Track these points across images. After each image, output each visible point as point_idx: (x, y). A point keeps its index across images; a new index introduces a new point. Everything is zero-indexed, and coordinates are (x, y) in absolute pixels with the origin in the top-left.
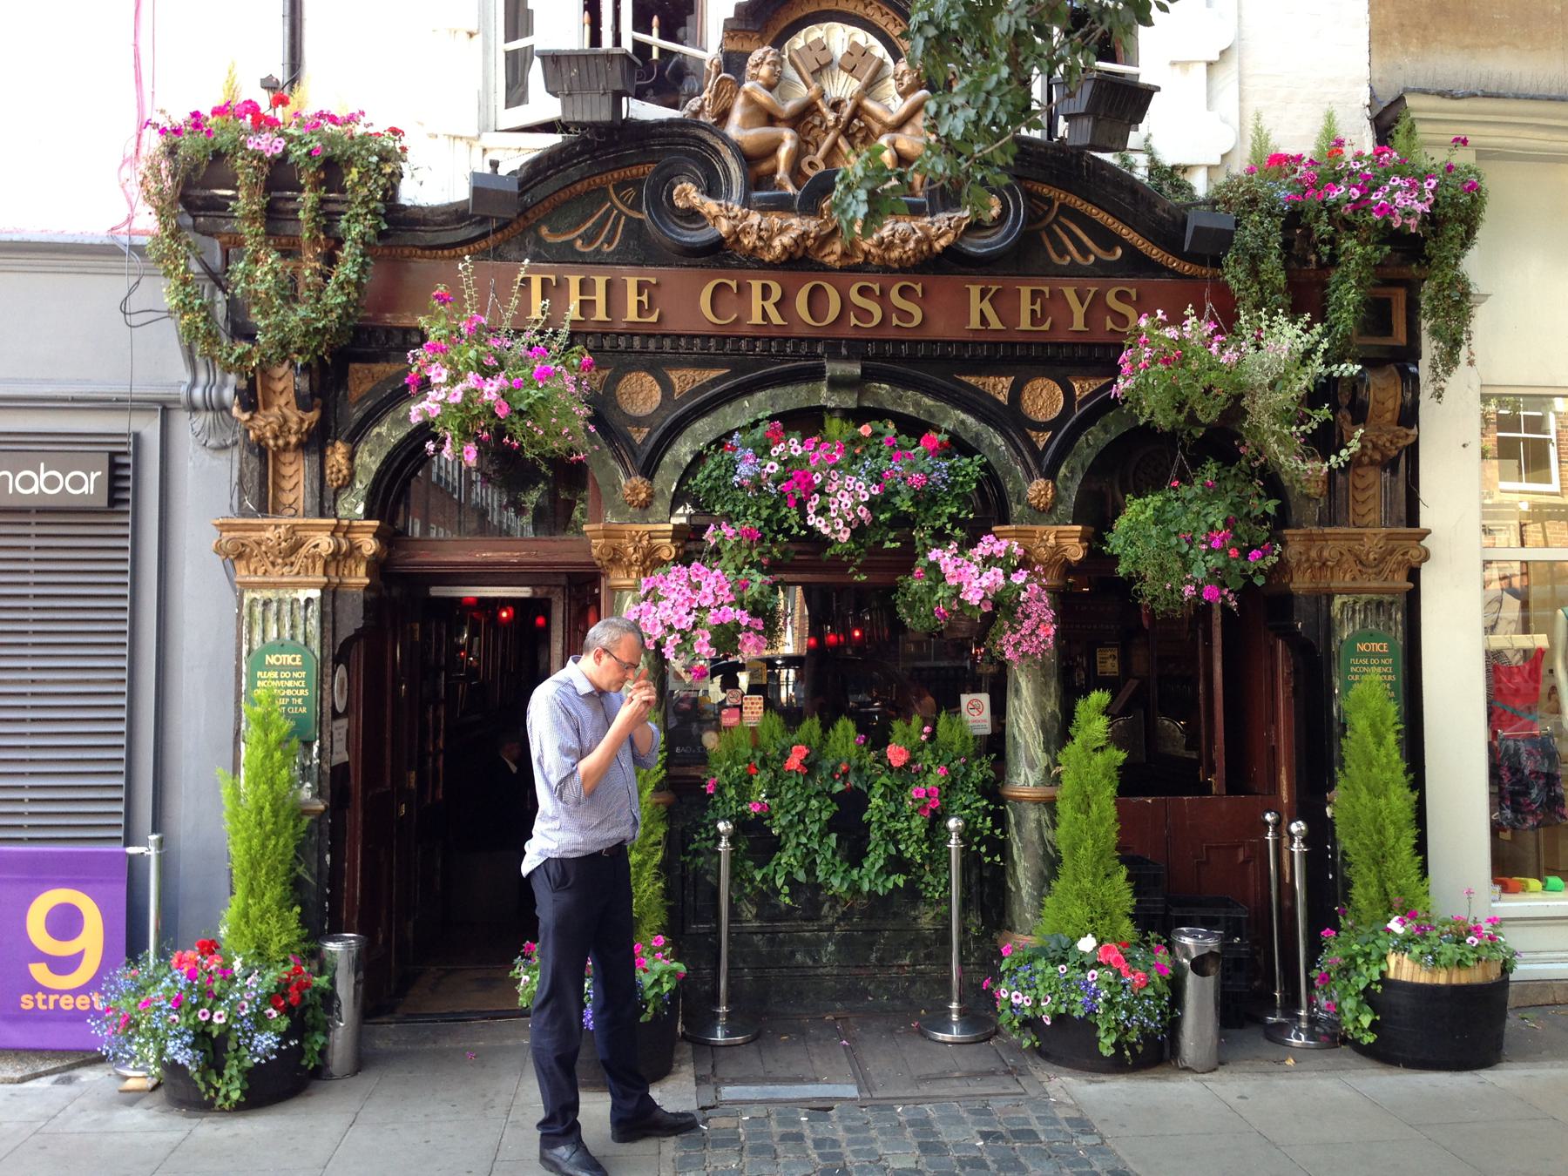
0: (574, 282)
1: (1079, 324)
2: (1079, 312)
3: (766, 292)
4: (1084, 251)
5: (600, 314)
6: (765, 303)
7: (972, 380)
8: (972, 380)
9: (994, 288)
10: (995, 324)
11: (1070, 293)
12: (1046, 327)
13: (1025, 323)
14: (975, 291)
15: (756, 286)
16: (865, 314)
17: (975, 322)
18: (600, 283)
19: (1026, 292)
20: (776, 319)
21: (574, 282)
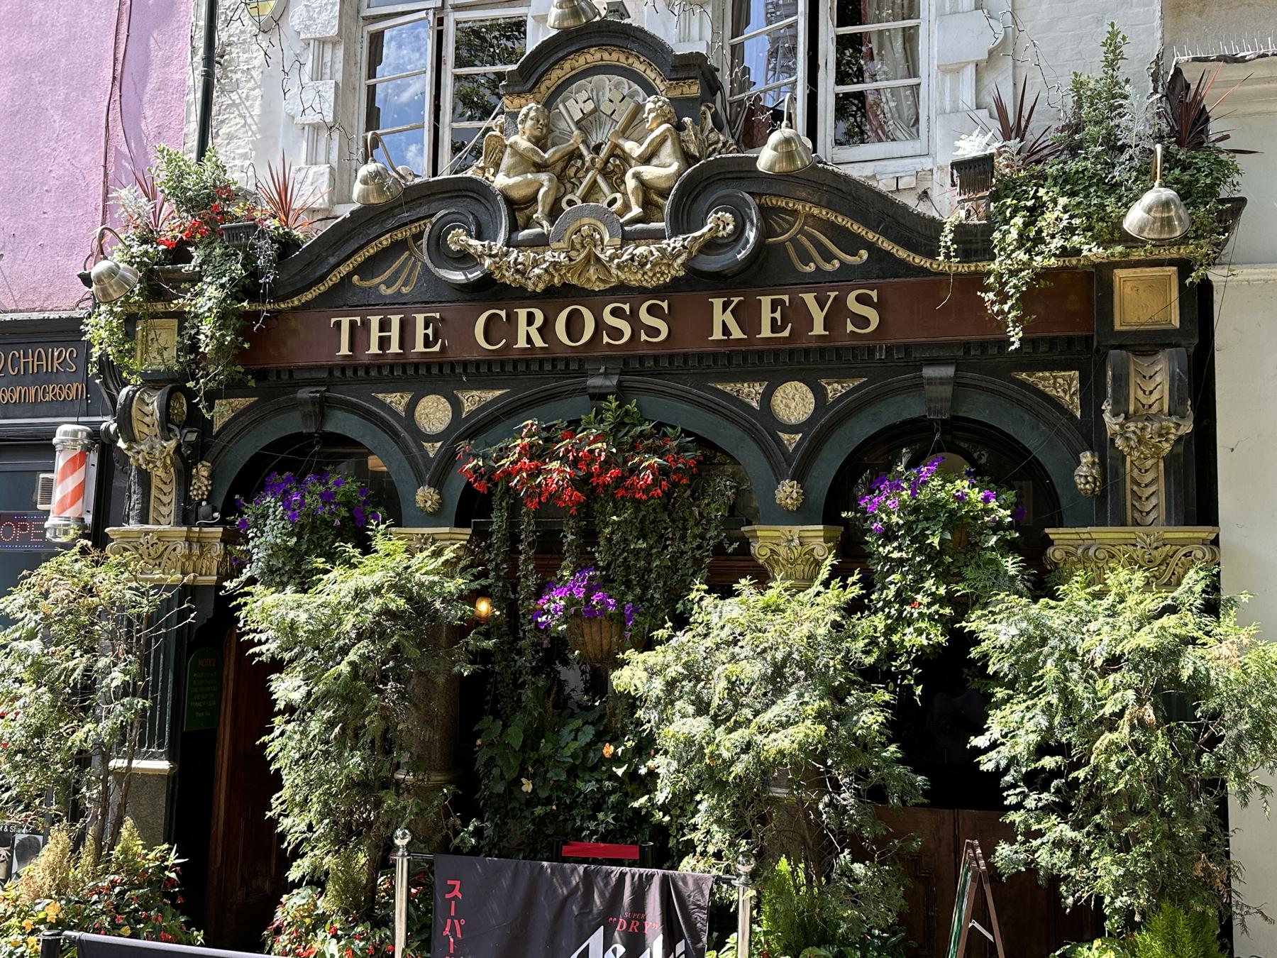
0: (375, 321)
1: (818, 329)
2: (818, 317)
3: (530, 319)
4: (829, 257)
5: (394, 348)
6: (529, 328)
7: (728, 388)
8: (728, 388)
9: (736, 300)
10: (737, 333)
11: (809, 299)
12: (786, 333)
13: (766, 332)
14: (718, 303)
15: (522, 314)
16: (617, 333)
17: (718, 335)
18: (395, 320)
19: (766, 301)
20: (539, 342)
21: (375, 321)
